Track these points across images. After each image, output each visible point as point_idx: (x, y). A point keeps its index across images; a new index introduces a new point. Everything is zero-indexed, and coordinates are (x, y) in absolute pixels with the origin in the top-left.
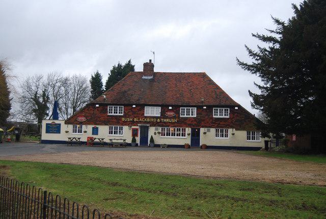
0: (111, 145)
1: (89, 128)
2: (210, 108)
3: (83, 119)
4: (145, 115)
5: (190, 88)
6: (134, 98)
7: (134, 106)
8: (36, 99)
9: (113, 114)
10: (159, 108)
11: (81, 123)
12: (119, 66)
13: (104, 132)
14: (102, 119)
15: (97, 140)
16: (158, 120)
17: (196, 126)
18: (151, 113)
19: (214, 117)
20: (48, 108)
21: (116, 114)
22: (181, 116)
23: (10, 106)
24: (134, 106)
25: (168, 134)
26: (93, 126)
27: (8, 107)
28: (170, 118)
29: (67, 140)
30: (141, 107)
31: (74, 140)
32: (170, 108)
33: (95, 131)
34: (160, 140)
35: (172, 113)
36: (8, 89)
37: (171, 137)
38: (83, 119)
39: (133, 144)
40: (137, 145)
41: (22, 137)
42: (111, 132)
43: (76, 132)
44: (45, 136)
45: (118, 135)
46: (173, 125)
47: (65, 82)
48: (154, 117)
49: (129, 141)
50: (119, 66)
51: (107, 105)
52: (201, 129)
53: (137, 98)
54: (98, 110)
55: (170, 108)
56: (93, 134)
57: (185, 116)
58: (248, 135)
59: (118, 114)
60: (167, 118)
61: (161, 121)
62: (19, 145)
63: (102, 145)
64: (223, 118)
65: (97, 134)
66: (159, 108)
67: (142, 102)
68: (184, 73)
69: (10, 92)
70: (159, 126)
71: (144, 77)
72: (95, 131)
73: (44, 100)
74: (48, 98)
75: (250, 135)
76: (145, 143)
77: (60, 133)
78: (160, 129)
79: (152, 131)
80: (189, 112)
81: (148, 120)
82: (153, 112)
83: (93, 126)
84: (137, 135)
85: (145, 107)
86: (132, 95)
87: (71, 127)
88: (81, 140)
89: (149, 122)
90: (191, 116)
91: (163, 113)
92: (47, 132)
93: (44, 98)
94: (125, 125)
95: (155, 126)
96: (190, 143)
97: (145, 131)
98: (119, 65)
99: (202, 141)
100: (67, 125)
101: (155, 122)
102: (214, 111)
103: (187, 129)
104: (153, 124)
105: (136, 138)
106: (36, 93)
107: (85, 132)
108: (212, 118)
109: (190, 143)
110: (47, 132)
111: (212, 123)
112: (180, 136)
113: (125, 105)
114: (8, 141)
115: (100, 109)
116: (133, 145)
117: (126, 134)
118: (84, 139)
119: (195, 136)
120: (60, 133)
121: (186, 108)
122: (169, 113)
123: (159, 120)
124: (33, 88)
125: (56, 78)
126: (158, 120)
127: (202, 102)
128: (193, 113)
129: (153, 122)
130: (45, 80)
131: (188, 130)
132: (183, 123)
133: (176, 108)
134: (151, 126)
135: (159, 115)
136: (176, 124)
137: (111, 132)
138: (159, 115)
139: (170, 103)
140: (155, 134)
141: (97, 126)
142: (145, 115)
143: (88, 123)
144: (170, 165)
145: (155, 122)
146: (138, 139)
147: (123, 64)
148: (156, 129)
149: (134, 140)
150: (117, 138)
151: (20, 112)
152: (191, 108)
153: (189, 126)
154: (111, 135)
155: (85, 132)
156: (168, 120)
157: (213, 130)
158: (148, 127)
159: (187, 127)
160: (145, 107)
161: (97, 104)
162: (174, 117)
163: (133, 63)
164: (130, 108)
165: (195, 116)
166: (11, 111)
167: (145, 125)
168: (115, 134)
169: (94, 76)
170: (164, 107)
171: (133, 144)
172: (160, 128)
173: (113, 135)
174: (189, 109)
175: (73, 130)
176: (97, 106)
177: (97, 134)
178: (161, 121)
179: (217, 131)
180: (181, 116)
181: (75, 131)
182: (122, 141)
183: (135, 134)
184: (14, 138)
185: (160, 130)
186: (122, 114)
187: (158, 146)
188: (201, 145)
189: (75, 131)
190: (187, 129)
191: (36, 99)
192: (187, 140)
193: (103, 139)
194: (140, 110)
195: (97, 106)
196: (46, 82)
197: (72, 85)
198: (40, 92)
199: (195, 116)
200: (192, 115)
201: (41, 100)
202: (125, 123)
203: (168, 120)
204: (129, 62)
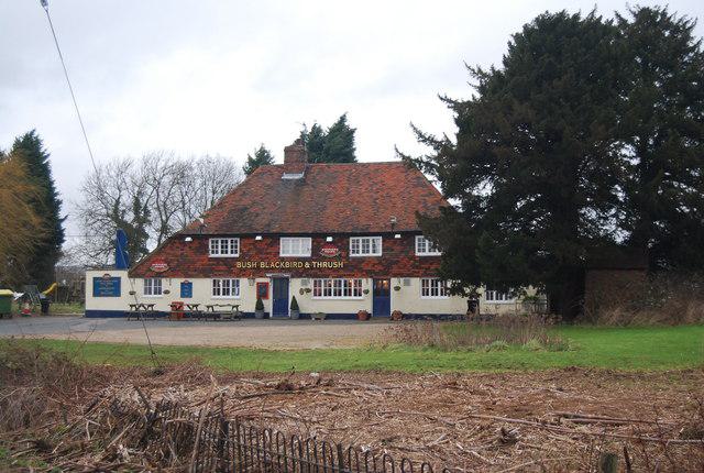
0: (214, 317)
1: (173, 285)
2: (409, 236)
3: (163, 266)
4: (282, 255)
5: (375, 196)
6: (260, 222)
7: (259, 238)
8: (116, 215)
9: (220, 255)
10: (308, 242)
11: (160, 275)
12: (316, 130)
13: (203, 292)
14: (198, 264)
15: (186, 308)
16: (307, 264)
17: (380, 271)
18: (293, 252)
19: (418, 254)
20: (147, 236)
22: (352, 255)
23: (63, 235)
24: (259, 238)
26: (183, 280)
27: (58, 237)
28: (330, 260)
29: (128, 309)
30: (273, 238)
31: (142, 308)
32: (329, 239)
33: (186, 290)
34: (309, 304)
35: (333, 250)
36: (56, 194)
37: (332, 297)
38: (163, 266)
39: (259, 314)
40: (266, 316)
41: (53, 306)
42: (216, 292)
43: (228, 294)
44: (93, 303)
45: (231, 296)
46: (336, 272)
47: (181, 174)
48: (298, 259)
49: (249, 306)
50: (316, 130)
51: (207, 237)
52: (392, 279)
53: (265, 222)
55: (329, 239)
56: (183, 295)
57: (361, 254)
59: (229, 255)
60: (323, 259)
61: (312, 268)
62: (46, 320)
63: (197, 316)
64: (425, 257)
66: (308, 242)
67: (275, 229)
68: (369, 164)
69: (60, 202)
70: (308, 276)
71: (286, 177)
72: (186, 290)
73: (137, 219)
74: (147, 212)
76: (285, 310)
78: (311, 284)
79: (295, 287)
80: (368, 246)
81: (287, 265)
82: (296, 248)
83: (183, 280)
84: (265, 296)
85: (282, 239)
86: (257, 215)
87: (139, 283)
88: (155, 308)
89: (289, 270)
90: (371, 254)
91: (315, 250)
92: (96, 293)
93: (136, 212)
94: (244, 276)
95: (300, 276)
96: (370, 311)
97: (281, 287)
98: (314, 127)
101: (301, 269)
102: (351, 244)
103: (364, 281)
104: (298, 274)
105: (264, 301)
106: (118, 202)
107: (167, 292)
108: (414, 257)
109: (370, 311)
110: (96, 293)
111: (414, 266)
112: (340, 295)
113: (242, 237)
114: (25, 315)
115: (193, 246)
116: (259, 315)
117: (245, 295)
118: (162, 304)
119: (381, 298)
121: (361, 239)
122: (327, 250)
123: (307, 265)
124: (111, 191)
125: (161, 164)
126: (307, 264)
127: (393, 224)
128: (375, 248)
129: (297, 269)
130: (137, 170)
131: (367, 284)
132: (357, 268)
133: (342, 239)
134: (293, 277)
135: (309, 255)
136: (342, 272)
137: (216, 292)
138: (309, 255)
139: (330, 230)
140: (302, 292)
141: (190, 280)
142: (282, 255)
143: (172, 273)
144: (184, 339)
145: (301, 269)
146: (268, 305)
147: (326, 125)
148: (304, 283)
149: (260, 306)
150: (223, 303)
151: (81, 249)
152: (371, 238)
153: (368, 274)
154: (217, 297)
155: (167, 292)
156: (325, 264)
157: (416, 282)
158: (287, 279)
159: (363, 276)
160: (282, 239)
161: (189, 236)
162: (339, 258)
163: (350, 123)
164: (251, 241)
165: (380, 254)
166: (65, 246)
167: (280, 275)
168: (345, 295)
169: (254, 157)
170: (318, 238)
171: (259, 314)
172: (312, 281)
173: (221, 296)
174: (368, 241)
175: (146, 289)
176: (188, 239)
178: (312, 268)
179: (424, 283)
180: (352, 255)
181: (147, 291)
182: (230, 309)
183: (262, 293)
184: (39, 308)
185: (311, 285)
186: (237, 255)
187: (306, 317)
189: (147, 291)
190: (364, 281)
191: (116, 215)
192: (365, 304)
193: (196, 306)
194: (271, 245)
195: (188, 239)
196: (139, 177)
197: (199, 182)
198: (127, 200)
199: (380, 254)
200: (374, 252)
201: (129, 217)
202: (243, 273)
203: (325, 264)
204: (343, 119)
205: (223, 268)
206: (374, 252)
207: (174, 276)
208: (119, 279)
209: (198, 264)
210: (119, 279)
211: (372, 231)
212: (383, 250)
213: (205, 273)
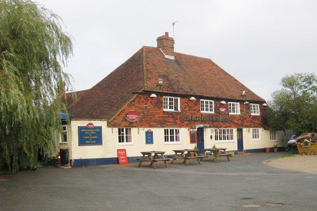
14: (157, 117)
21: (206, 100)
25: (225, 139)
33: (149, 139)
43: (123, 141)
54: (151, 102)
58: (165, 134)
65: (79, 127)
72: (149, 139)
75: (168, 134)
77: (101, 127)
79: (208, 133)
83: (146, 129)
92: (82, 142)
99: (246, 146)
100: (110, 129)
108: (251, 115)
110: (82, 142)
120: (101, 127)
121: (168, 98)
141: (152, 129)
143: (140, 124)
168: (171, 141)
175: (120, 137)
177: (79, 127)
188: (244, 149)
199: (239, 113)
205: (171, 120)
206: (234, 111)
207: (141, 126)
208: (100, 128)
209: (157, 117)
210: (100, 128)
211: (205, 95)
212: (241, 111)
213: (161, 124)
